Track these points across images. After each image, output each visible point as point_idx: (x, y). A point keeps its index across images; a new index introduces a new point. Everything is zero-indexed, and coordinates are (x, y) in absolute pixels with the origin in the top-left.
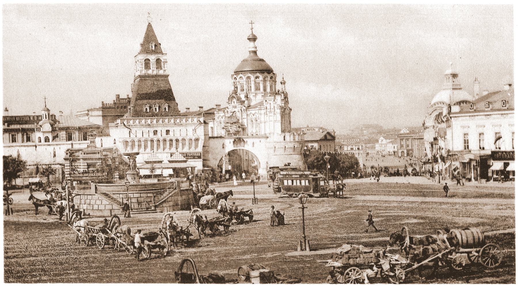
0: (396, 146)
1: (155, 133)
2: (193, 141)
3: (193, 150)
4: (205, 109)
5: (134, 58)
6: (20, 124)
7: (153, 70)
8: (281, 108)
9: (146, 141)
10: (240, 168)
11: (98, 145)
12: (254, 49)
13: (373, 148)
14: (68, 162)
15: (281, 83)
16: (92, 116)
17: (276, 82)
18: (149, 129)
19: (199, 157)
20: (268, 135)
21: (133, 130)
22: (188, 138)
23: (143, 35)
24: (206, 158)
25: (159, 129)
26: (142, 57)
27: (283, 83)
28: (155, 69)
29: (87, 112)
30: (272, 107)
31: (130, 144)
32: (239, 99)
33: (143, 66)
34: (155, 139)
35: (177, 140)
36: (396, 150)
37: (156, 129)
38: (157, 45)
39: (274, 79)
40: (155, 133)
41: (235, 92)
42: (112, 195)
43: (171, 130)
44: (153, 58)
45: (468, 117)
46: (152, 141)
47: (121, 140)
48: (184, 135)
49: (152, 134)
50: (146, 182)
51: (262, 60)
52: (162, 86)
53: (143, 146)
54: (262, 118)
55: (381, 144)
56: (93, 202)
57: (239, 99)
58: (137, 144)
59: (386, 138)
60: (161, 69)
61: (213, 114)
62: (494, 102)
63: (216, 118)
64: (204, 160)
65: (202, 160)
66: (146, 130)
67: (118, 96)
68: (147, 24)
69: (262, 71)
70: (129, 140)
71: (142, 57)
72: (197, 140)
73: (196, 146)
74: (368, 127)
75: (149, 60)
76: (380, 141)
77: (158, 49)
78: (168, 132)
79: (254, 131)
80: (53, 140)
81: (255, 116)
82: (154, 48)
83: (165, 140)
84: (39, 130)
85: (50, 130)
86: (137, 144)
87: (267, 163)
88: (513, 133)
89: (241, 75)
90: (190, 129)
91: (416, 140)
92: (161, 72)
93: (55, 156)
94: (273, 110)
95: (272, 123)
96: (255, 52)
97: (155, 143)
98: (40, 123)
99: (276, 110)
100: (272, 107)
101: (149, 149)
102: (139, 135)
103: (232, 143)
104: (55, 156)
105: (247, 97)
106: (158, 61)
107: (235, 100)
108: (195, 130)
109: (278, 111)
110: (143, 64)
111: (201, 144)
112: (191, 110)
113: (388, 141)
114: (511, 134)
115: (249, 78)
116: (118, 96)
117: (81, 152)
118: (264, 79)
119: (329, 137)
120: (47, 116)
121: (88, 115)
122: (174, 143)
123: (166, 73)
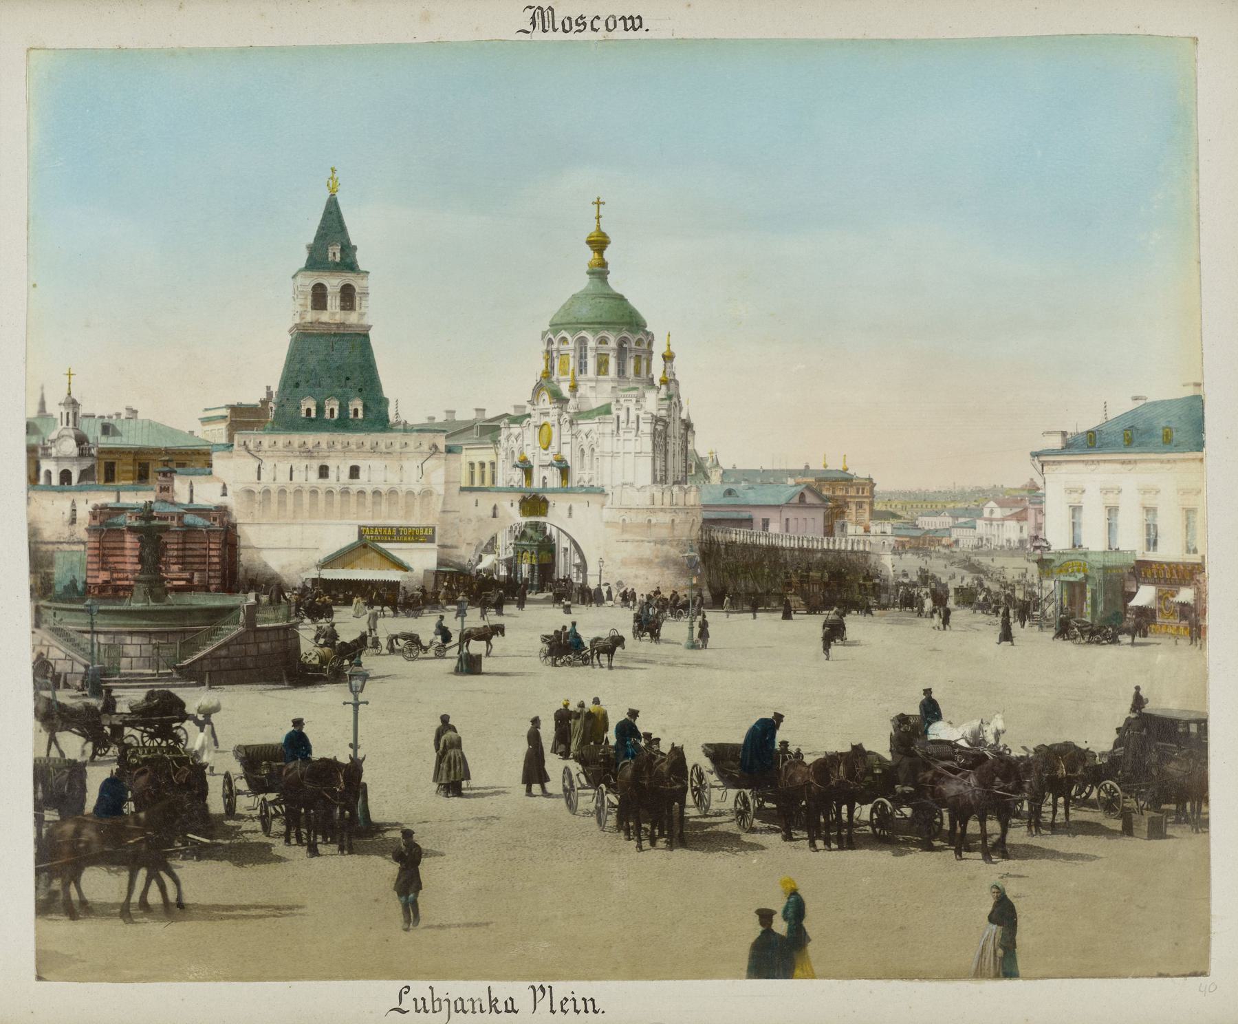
1: (324, 472)
4: (488, 415)
5: (291, 281)
17: (651, 353)
18: (306, 462)
21: (268, 465)
22: (404, 488)
25: (332, 464)
26: (310, 280)
27: (668, 358)
28: (338, 310)
30: (633, 417)
34: (291, 488)
38: (348, 250)
39: (645, 346)
40: (324, 472)
41: (548, 374)
42: (74, 635)
44: (333, 283)
45: (1118, 466)
47: (238, 487)
49: (314, 475)
50: (194, 602)
51: (621, 298)
54: (607, 444)
62: (1173, 430)
63: (502, 438)
64: (442, 546)
66: (300, 464)
70: (257, 488)
71: (310, 280)
72: (427, 493)
76: (986, 513)
77: (348, 264)
78: (354, 472)
79: (586, 478)
88: (599, 244)
90: (411, 466)
92: (352, 318)
94: (634, 426)
99: (642, 426)
100: (633, 417)
102: (283, 478)
103: (517, 505)
107: (546, 397)
109: (646, 428)
110: (310, 298)
113: (1008, 512)
114: (1069, 513)
118: (620, 345)
120: (71, 418)
123: (366, 321)
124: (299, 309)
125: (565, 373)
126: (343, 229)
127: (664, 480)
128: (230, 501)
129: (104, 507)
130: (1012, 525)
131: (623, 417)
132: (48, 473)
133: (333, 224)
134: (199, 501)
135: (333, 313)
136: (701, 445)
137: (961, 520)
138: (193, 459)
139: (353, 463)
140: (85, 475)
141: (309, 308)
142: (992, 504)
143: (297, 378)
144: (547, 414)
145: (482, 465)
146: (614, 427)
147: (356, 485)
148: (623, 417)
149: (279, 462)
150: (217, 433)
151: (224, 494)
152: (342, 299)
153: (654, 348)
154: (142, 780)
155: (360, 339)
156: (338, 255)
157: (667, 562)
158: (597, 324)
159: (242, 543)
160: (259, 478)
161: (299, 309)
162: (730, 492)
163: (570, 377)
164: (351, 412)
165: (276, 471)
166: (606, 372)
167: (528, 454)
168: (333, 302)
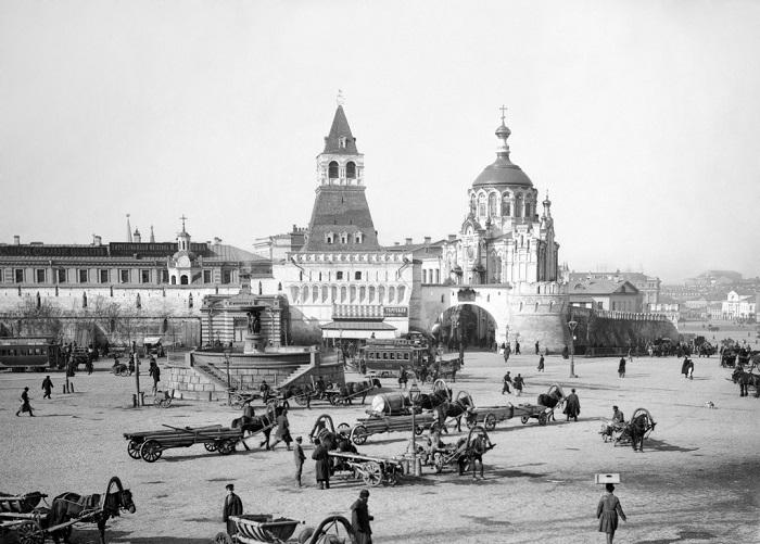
0: (754, 305)
1: (339, 275)
2: (396, 290)
3: (394, 303)
4: (433, 241)
6: (155, 256)
8: (540, 242)
9: (325, 287)
10: (473, 332)
11: (255, 291)
12: (504, 151)
13: (720, 306)
14: (206, 314)
16: (276, 246)
17: (536, 202)
19: (405, 315)
20: (511, 284)
21: (307, 271)
22: (389, 284)
23: (330, 127)
24: (415, 317)
25: (345, 271)
27: (547, 204)
29: (269, 240)
30: (525, 241)
31: (301, 291)
32: (477, 227)
35: (372, 288)
36: (753, 312)
38: (351, 141)
40: (339, 275)
41: (472, 216)
44: (342, 161)
46: (334, 288)
47: (288, 284)
48: (382, 279)
49: (334, 278)
51: (516, 168)
52: (355, 203)
53: (320, 295)
56: (187, 380)
57: (477, 227)
58: (311, 291)
59: (740, 293)
61: (440, 248)
63: (444, 254)
64: (411, 319)
65: (407, 318)
66: (325, 270)
68: (337, 107)
69: (513, 185)
71: (327, 159)
73: (401, 298)
74: (718, 274)
75: (336, 163)
76: (729, 299)
78: (358, 275)
80: (193, 281)
83: (353, 288)
84: (172, 266)
86: (311, 291)
87: (508, 327)
88: (504, 133)
89: (481, 190)
92: (354, 182)
93: (191, 305)
95: (523, 266)
96: (506, 155)
97: (339, 292)
98: (176, 255)
100: (525, 241)
101: (310, 298)
102: (316, 278)
103: (456, 295)
104: (191, 305)
107: (471, 229)
108: (399, 273)
109: (534, 247)
110: (328, 168)
111: (407, 294)
112: (414, 242)
115: (493, 194)
117: (225, 301)
118: (517, 197)
119: (628, 290)
121: (270, 244)
122: (367, 292)
123: (362, 184)
124: (321, 177)
125: (483, 214)
127: (544, 279)
128: (286, 292)
129: (210, 297)
130: (746, 304)
131: (519, 242)
132: (174, 277)
134: (266, 293)
135: (341, 180)
136: (563, 258)
137: (713, 302)
138: (263, 268)
140: (195, 278)
142: (733, 293)
143: (322, 217)
144: (471, 240)
145: (431, 270)
147: (358, 284)
148: (519, 242)
149: (318, 270)
150: (280, 254)
151: (280, 289)
152: (347, 171)
153: (538, 199)
155: (359, 192)
157: (537, 329)
158: (500, 185)
159: (293, 317)
161: (321, 177)
162: (578, 286)
166: (508, 214)
167: (460, 264)
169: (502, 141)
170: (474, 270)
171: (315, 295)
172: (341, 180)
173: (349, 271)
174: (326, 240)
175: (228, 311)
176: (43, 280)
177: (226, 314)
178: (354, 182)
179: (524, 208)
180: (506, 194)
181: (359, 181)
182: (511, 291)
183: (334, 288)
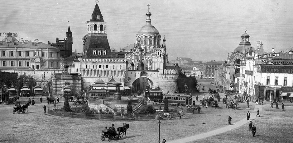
7: (98, 31)
15: (163, 40)
26: (93, 23)
27: (164, 41)
30: (159, 54)
32: (140, 48)
33: (93, 28)
37: (101, 64)
38: (101, 17)
40: (100, 66)
41: (138, 44)
43: (109, 65)
44: (98, 24)
46: (98, 71)
49: (98, 67)
55: (194, 71)
60: (103, 30)
67: (57, 39)
77: (101, 20)
78: (107, 67)
81: (149, 59)
82: (99, 19)
85: (40, 61)
88: (149, 15)
91: (218, 71)
92: (103, 32)
93: (44, 77)
94: (160, 56)
100: (159, 54)
101: (89, 75)
102: (92, 68)
105: (145, 48)
106: (102, 26)
115: (146, 37)
116: (57, 39)
123: (105, 33)
126: (99, 12)
128: (79, 72)
131: (157, 54)
133: (97, 11)
135: (98, 31)
139: (107, 65)
141: (93, 30)
144: (138, 53)
146: (155, 56)
148: (157, 54)
151: (77, 71)
154: (207, 103)
156: (99, 18)
160: (86, 68)
163: (144, 45)
164: (99, 53)
165: (90, 66)
168: (98, 28)
169: (148, 17)
170: (140, 64)
171: (88, 73)
172: (98, 31)
173: (104, 65)
174: (94, 54)
175: (63, 80)
176: (5, 55)
177: (62, 81)
178: (103, 32)
179: (157, 42)
180: (151, 37)
181: (105, 32)
182: (159, 73)
183: (98, 71)
